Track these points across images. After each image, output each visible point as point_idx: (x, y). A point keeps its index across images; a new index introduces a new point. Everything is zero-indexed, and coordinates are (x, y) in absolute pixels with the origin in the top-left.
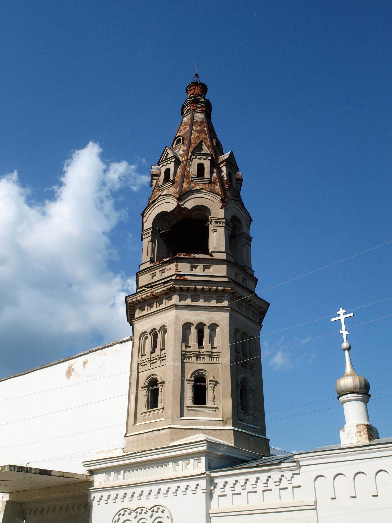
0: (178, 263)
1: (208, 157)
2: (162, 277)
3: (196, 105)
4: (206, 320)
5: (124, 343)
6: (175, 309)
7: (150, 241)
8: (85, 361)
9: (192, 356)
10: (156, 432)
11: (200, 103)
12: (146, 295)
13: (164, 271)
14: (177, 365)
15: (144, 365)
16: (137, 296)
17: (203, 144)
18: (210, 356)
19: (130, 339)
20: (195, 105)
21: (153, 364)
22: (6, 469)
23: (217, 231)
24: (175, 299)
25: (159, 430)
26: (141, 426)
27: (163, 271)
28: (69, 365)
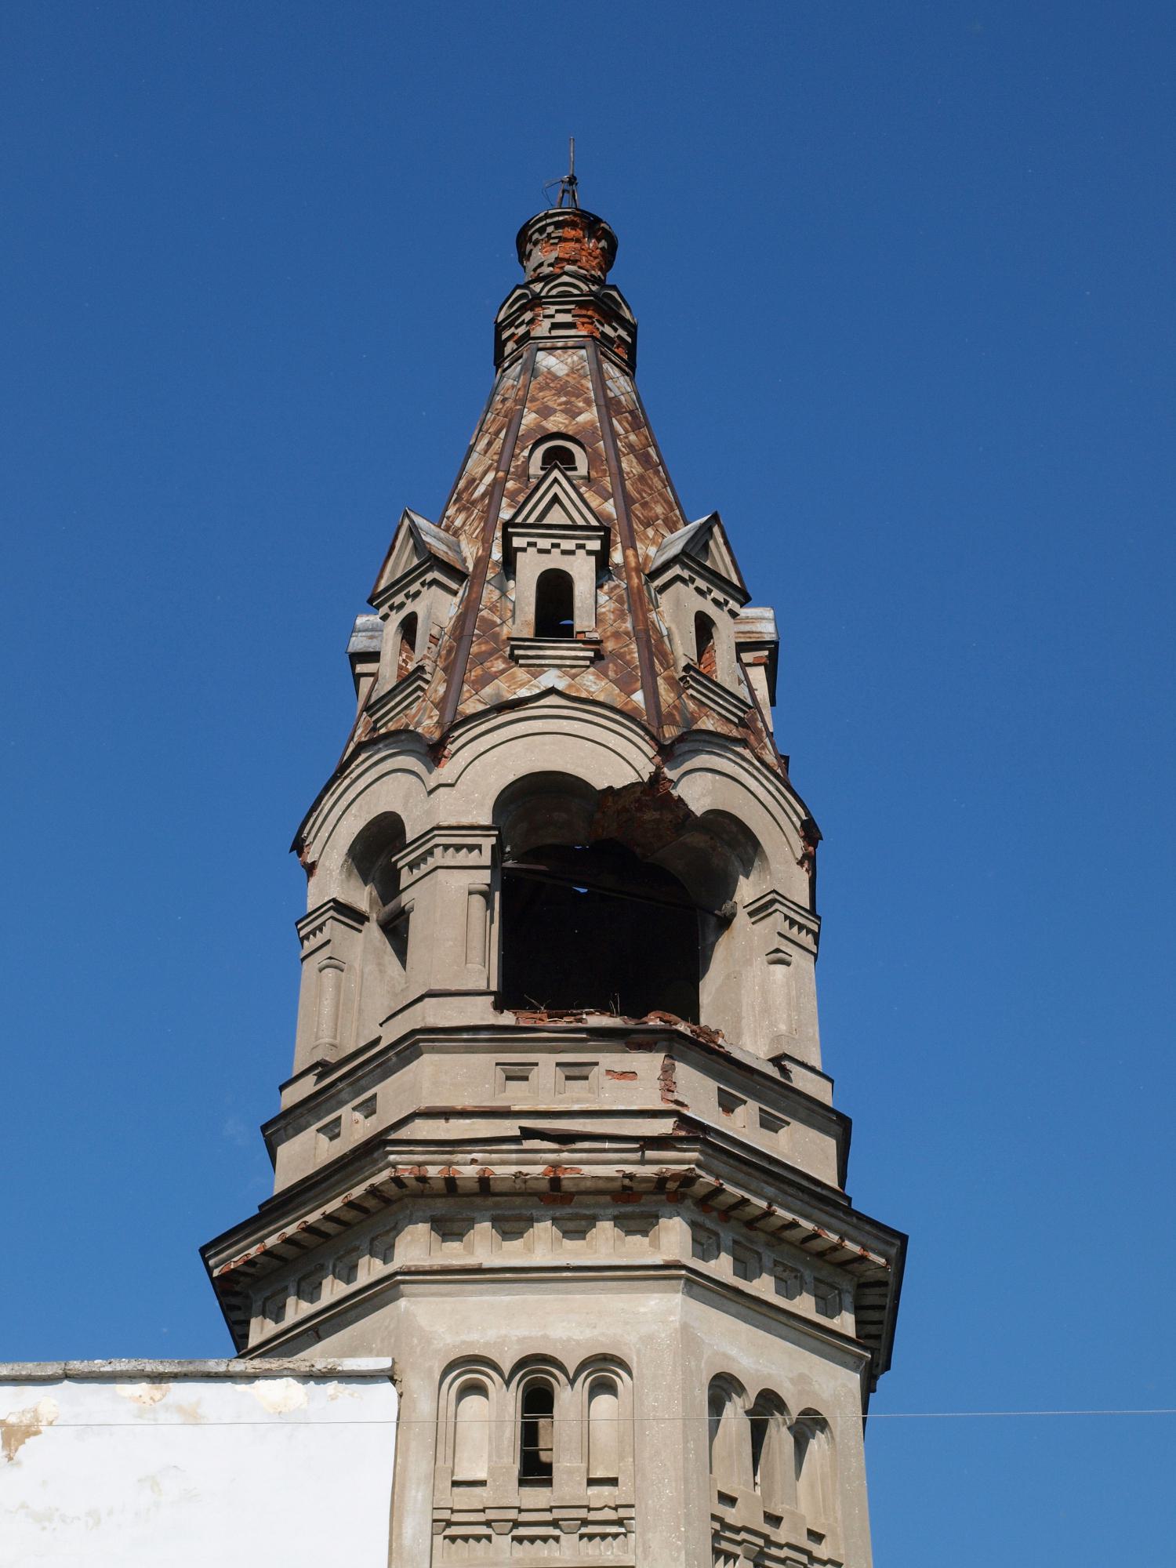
0: (675, 1060)
1: (731, 602)
4: (787, 1384)
5: (332, 1387)
9: (738, 1550)
11: (618, 324)
12: (514, 1169)
16: (459, 1157)
17: (716, 530)
19: (389, 1373)
23: (788, 964)
27: (576, 1071)
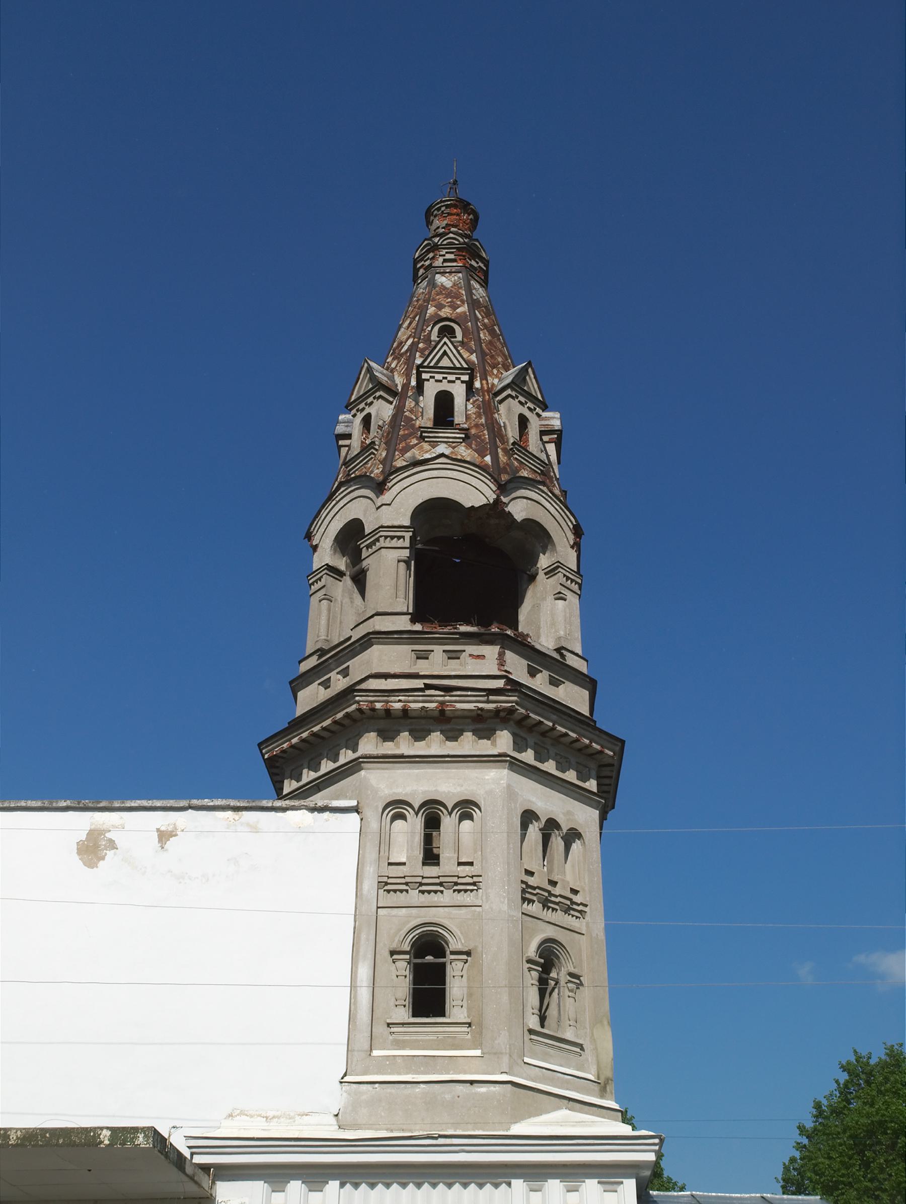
2: (445, 670)
3: (471, 258)
4: (561, 816)
5: (327, 815)
6: (507, 766)
7: (404, 561)
8: (163, 829)
9: (535, 898)
10: (461, 1087)
12: (421, 705)
13: (458, 656)
14: (514, 914)
15: (395, 891)
16: (392, 698)
18: (567, 910)
19: (356, 808)
20: (468, 258)
21: (426, 893)
22: (141, 1139)
23: (565, 600)
24: (503, 741)
25: (472, 1082)
26: (399, 1060)
27: (454, 655)
28: (92, 824)
